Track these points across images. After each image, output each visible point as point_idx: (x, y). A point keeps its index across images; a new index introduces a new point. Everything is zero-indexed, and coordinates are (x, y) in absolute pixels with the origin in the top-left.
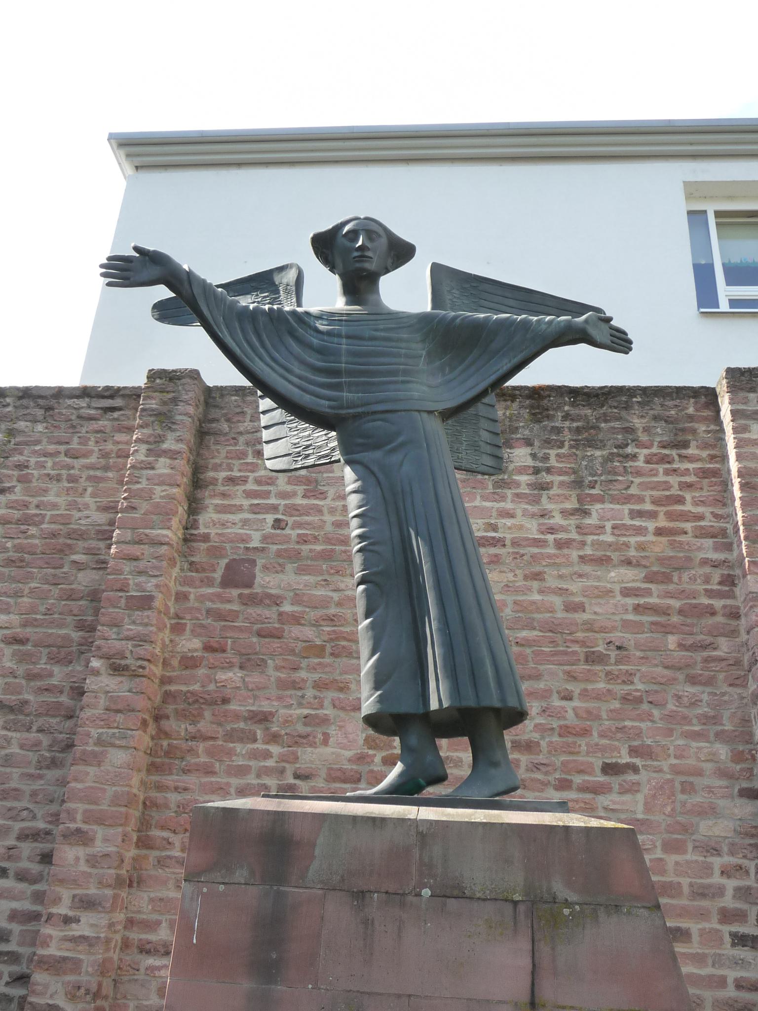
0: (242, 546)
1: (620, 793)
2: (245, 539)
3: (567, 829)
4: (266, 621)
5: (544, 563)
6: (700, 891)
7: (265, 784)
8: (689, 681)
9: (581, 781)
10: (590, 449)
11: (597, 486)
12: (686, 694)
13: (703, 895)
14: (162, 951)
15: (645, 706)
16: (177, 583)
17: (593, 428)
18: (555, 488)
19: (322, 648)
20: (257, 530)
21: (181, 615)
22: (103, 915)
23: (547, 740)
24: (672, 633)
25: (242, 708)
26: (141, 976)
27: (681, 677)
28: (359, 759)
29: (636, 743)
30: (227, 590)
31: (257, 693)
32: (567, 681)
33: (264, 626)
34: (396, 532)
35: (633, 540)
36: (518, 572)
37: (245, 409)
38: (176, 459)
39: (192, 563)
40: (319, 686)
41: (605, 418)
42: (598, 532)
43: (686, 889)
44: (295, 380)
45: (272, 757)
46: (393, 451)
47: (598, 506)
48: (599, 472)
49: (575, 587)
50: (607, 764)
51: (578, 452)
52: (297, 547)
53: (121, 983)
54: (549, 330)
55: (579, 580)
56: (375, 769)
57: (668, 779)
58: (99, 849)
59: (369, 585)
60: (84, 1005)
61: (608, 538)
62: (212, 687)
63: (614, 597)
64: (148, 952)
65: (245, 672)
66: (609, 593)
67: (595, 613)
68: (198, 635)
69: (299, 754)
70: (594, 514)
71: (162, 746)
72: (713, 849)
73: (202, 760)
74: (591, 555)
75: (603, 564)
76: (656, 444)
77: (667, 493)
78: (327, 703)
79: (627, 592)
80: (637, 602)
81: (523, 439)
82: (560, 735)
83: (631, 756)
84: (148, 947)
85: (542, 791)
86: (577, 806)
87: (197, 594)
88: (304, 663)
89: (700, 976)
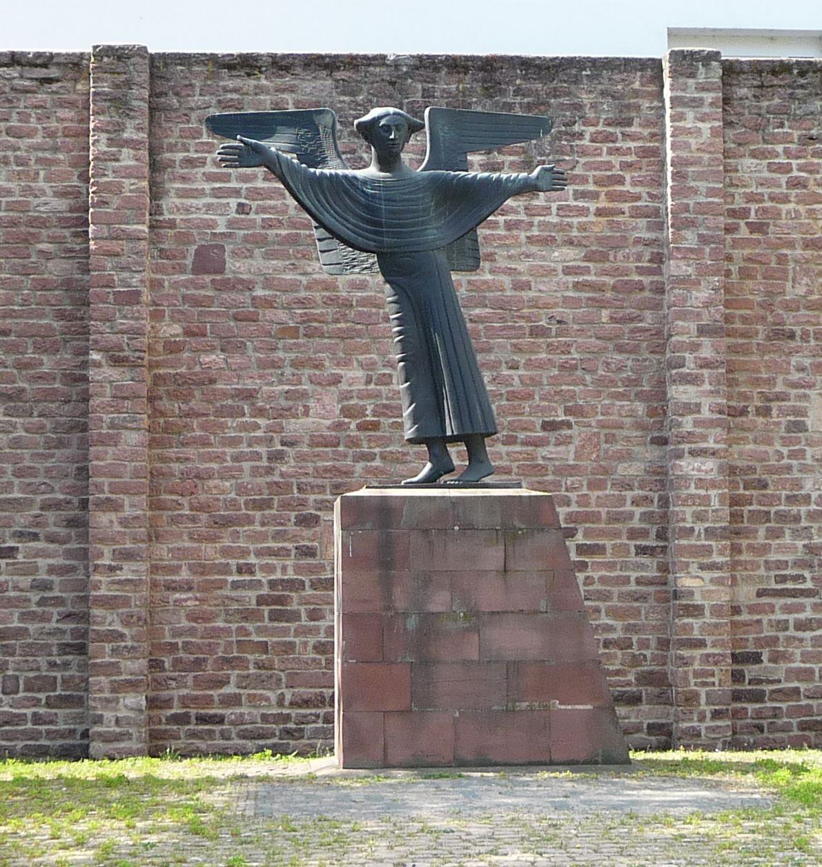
0: (209, 231)
2: (212, 225)
13: (617, 520)
14: (186, 587)
15: (579, 373)
17: (542, 104)
27: (611, 346)
30: (200, 277)
35: (575, 221)
37: (194, 81)
39: (161, 250)
40: (296, 364)
41: (555, 93)
43: (604, 516)
61: (555, 220)
62: (197, 369)
63: (557, 275)
64: (174, 589)
73: (198, 434)
76: (602, 121)
77: (609, 173)
79: (568, 271)
84: (173, 585)
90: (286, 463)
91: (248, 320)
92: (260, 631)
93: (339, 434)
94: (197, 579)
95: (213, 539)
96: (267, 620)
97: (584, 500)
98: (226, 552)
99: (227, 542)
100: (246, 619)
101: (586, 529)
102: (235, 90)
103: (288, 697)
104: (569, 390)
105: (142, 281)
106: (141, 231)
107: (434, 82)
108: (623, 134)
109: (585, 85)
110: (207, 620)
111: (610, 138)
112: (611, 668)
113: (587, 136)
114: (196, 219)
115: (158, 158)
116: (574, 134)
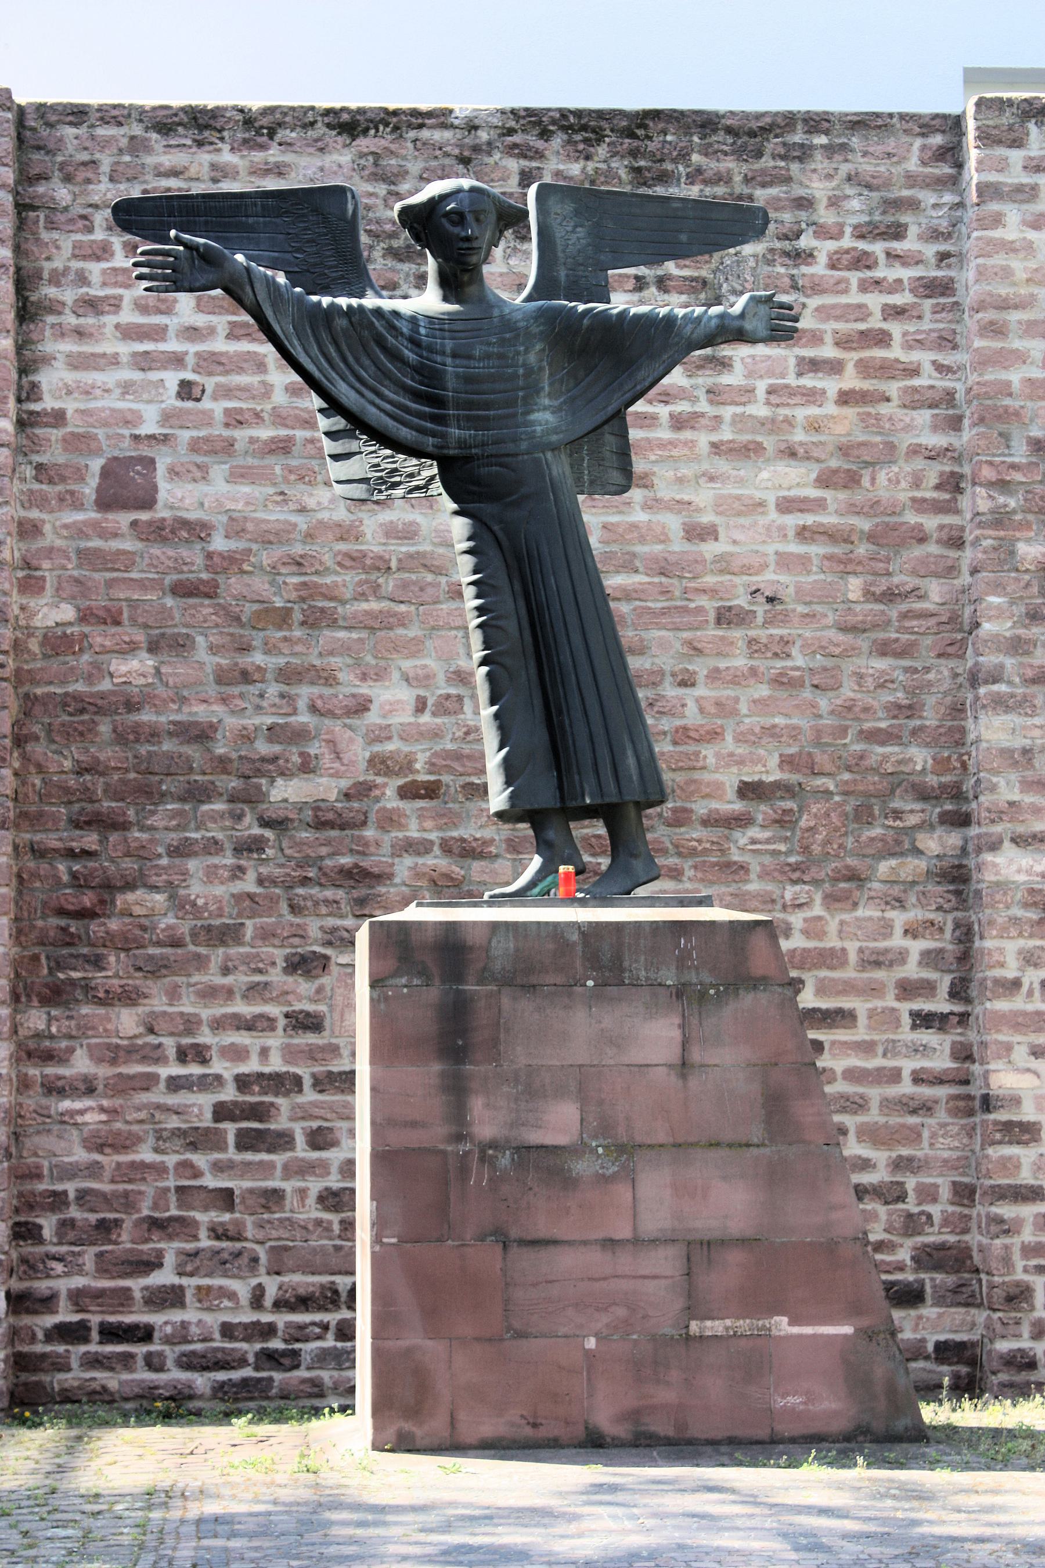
0: (126, 432)
2: (130, 419)
3: (712, 923)
4: (185, 568)
5: (653, 458)
12: (871, 671)
13: (878, 964)
14: (82, 1087)
19: (288, 612)
21: (34, 563)
30: (110, 516)
34: (521, 603)
35: (801, 413)
37: (97, 156)
39: (39, 467)
42: (744, 399)
43: (853, 957)
49: (703, 496)
50: (745, 783)
52: (226, 433)
56: (389, 806)
61: (759, 410)
62: (105, 685)
67: (735, 542)
70: (738, 366)
74: (731, 441)
75: (749, 457)
76: (848, 230)
77: (862, 326)
78: (302, 704)
79: (787, 506)
80: (801, 523)
82: (675, 743)
84: (60, 1083)
88: (257, 639)
92: (218, 1168)
94: (104, 1071)
96: (231, 1148)
100: (193, 1146)
103: (271, 1293)
108: (888, 254)
110: (125, 1148)
111: (862, 261)
114: (103, 409)
115: (34, 298)
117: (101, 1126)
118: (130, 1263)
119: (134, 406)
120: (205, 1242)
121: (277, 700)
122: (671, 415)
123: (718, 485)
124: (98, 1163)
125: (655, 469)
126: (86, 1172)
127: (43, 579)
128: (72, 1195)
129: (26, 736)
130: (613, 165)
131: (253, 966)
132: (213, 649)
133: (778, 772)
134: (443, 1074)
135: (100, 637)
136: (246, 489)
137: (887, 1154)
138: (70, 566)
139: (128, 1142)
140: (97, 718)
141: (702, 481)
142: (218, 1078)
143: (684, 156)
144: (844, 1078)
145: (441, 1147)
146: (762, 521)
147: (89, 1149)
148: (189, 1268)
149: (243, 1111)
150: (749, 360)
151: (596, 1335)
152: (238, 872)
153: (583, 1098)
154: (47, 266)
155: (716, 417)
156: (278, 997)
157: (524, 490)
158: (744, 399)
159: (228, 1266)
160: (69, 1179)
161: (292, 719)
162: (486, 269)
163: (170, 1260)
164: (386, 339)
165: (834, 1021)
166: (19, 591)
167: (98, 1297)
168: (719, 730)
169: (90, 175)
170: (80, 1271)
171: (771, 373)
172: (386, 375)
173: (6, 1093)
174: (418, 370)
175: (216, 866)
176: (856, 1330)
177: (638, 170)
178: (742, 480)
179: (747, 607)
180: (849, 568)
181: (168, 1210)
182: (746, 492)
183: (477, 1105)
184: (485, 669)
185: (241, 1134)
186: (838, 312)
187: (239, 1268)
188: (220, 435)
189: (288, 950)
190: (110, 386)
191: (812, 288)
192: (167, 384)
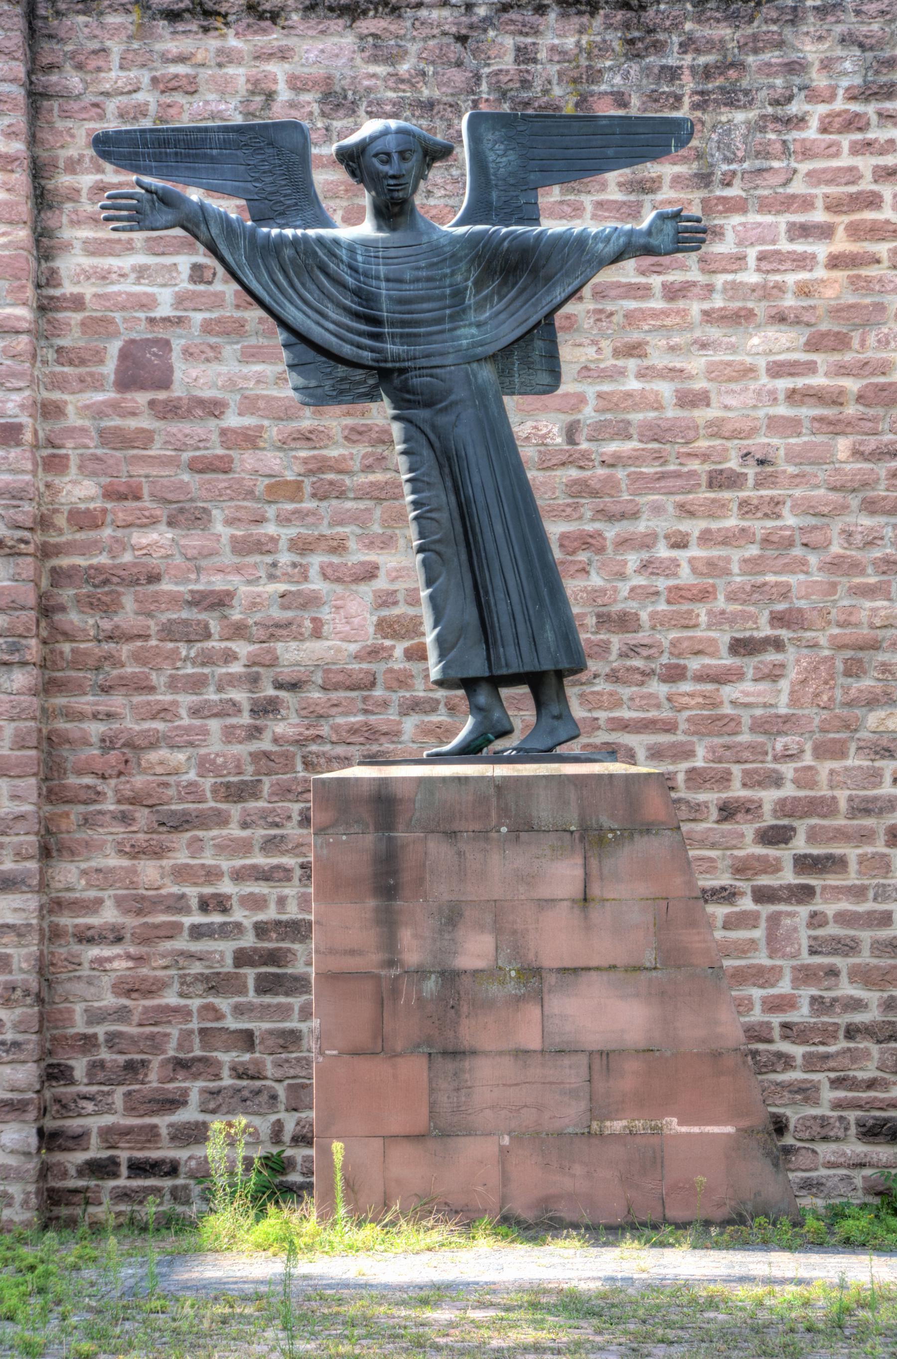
0: (142, 315)
1: (756, 680)
2: (146, 303)
3: (611, 776)
4: (201, 445)
5: (646, 327)
6: (862, 806)
7: (231, 700)
8: (866, 509)
9: (698, 667)
10: (727, 109)
11: (737, 182)
12: (860, 529)
13: (867, 812)
14: (111, 937)
15: (798, 551)
16: (41, 387)
17: (732, 65)
18: (665, 188)
19: (298, 485)
20: (164, 285)
21: (58, 442)
22: (29, 896)
23: (650, 609)
24: (843, 433)
25: (181, 588)
26: (85, 972)
27: (854, 501)
28: (369, 653)
29: (781, 607)
30: (128, 396)
31: (203, 563)
32: (679, 518)
33: (198, 453)
34: (453, 499)
35: (791, 279)
36: (604, 344)
37: (108, 43)
38: (12, 171)
39: (59, 350)
40: (302, 546)
41: (755, 45)
42: (735, 267)
43: (843, 805)
44: (331, 327)
45: (236, 658)
46: (445, 410)
47: (736, 219)
48: (740, 154)
49: (696, 364)
50: (737, 640)
51: (705, 117)
52: (237, 314)
53: (58, 983)
54: (607, 249)
55: (701, 353)
56: (396, 667)
57: (826, 657)
58: (7, 810)
59: (428, 554)
60: (25, 1009)
61: (751, 277)
62: (127, 557)
63: (756, 379)
64: (90, 941)
65: (180, 532)
66: (748, 372)
67: (726, 407)
68: (94, 474)
69: (279, 652)
70: (730, 236)
71: (61, 653)
72: (883, 749)
73: (129, 670)
74: (722, 309)
75: (740, 324)
76: (841, 92)
77: (853, 189)
78: (314, 572)
79: (777, 370)
80: (791, 386)
81: (612, 93)
82: (669, 602)
83: (773, 627)
84: (90, 933)
85: (642, 684)
86: (693, 702)
87: (80, 404)
88: (271, 511)
89: (856, 913)
90: (283, 719)
91: (214, 471)
92: (239, 1011)
93: (373, 667)
94: (131, 922)
95: (158, 852)
96: (251, 993)
97: (806, 778)
98: (181, 873)
99: (182, 858)
100: (212, 989)
101: (812, 828)
102: (181, 59)
103: (290, 1128)
104: (777, 584)
105: (22, 407)
106: (18, 318)
107: (537, 33)
108: (880, 114)
109: (811, 24)
110: (149, 993)
111: (854, 123)
112: (861, 1075)
113: (814, 123)
114: (119, 293)
115: (50, 185)
116: (789, 120)
117: (128, 973)
118: (157, 1101)
119: (149, 290)
120: (227, 1081)
121: (289, 570)
122: (664, 285)
123: (711, 353)
124: (126, 1007)
125: (648, 338)
126: (115, 1016)
127: (67, 457)
128: (101, 1038)
129: (53, 607)
130: (608, 37)
131: (270, 820)
132: (230, 522)
133: (768, 628)
134: (377, 910)
135: (121, 511)
136: (258, 368)
137: (878, 994)
138: (92, 445)
139: (154, 988)
140: (120, 589)
141: (694, 348)
142: (238, 926)
143: (676, 26)
144: (836, 922)
145: (376, 971)
146: (753, 385)
147: (117, 994)
148: (212, 1106)
149: (261, 956)
150: (740, 228)
151: (509, 1134)
152: (255, 732)
153: (498, 930)
154: (63, 154)
155: (708, 285)
156: (293, 848)
157: (453, 397)
158: (735, 267)
159: (248, 1103)
160: (98, 1023)
161: (304, 587)
162: (418, 200)
163: (194, 1097)
164: (328, 266)
165: (825, 867)
166: (44, 470)
167: (127, 1134)
168: (710, 589)
169: (101, 63)
170: (110, 1110)
171: (762, 241)
172: (330, 297)
173: (35, 942)
174: (357, 293)
175: (233, 727)
176: (738, 1130)
177: (631, 42)
178: (733, 346)
179: (739, 470)
180: (838, 429)
181: (192, 1051)
182: (738, 358)
183: (405, 935)
184: (420, 556)
185: (259, 978)
186: (829, 176)
187: (259, 1105)
188: (232, 317)
189: (302, 805)
190: (127, 270)
191: (803, 154)
192: (180, 268)
